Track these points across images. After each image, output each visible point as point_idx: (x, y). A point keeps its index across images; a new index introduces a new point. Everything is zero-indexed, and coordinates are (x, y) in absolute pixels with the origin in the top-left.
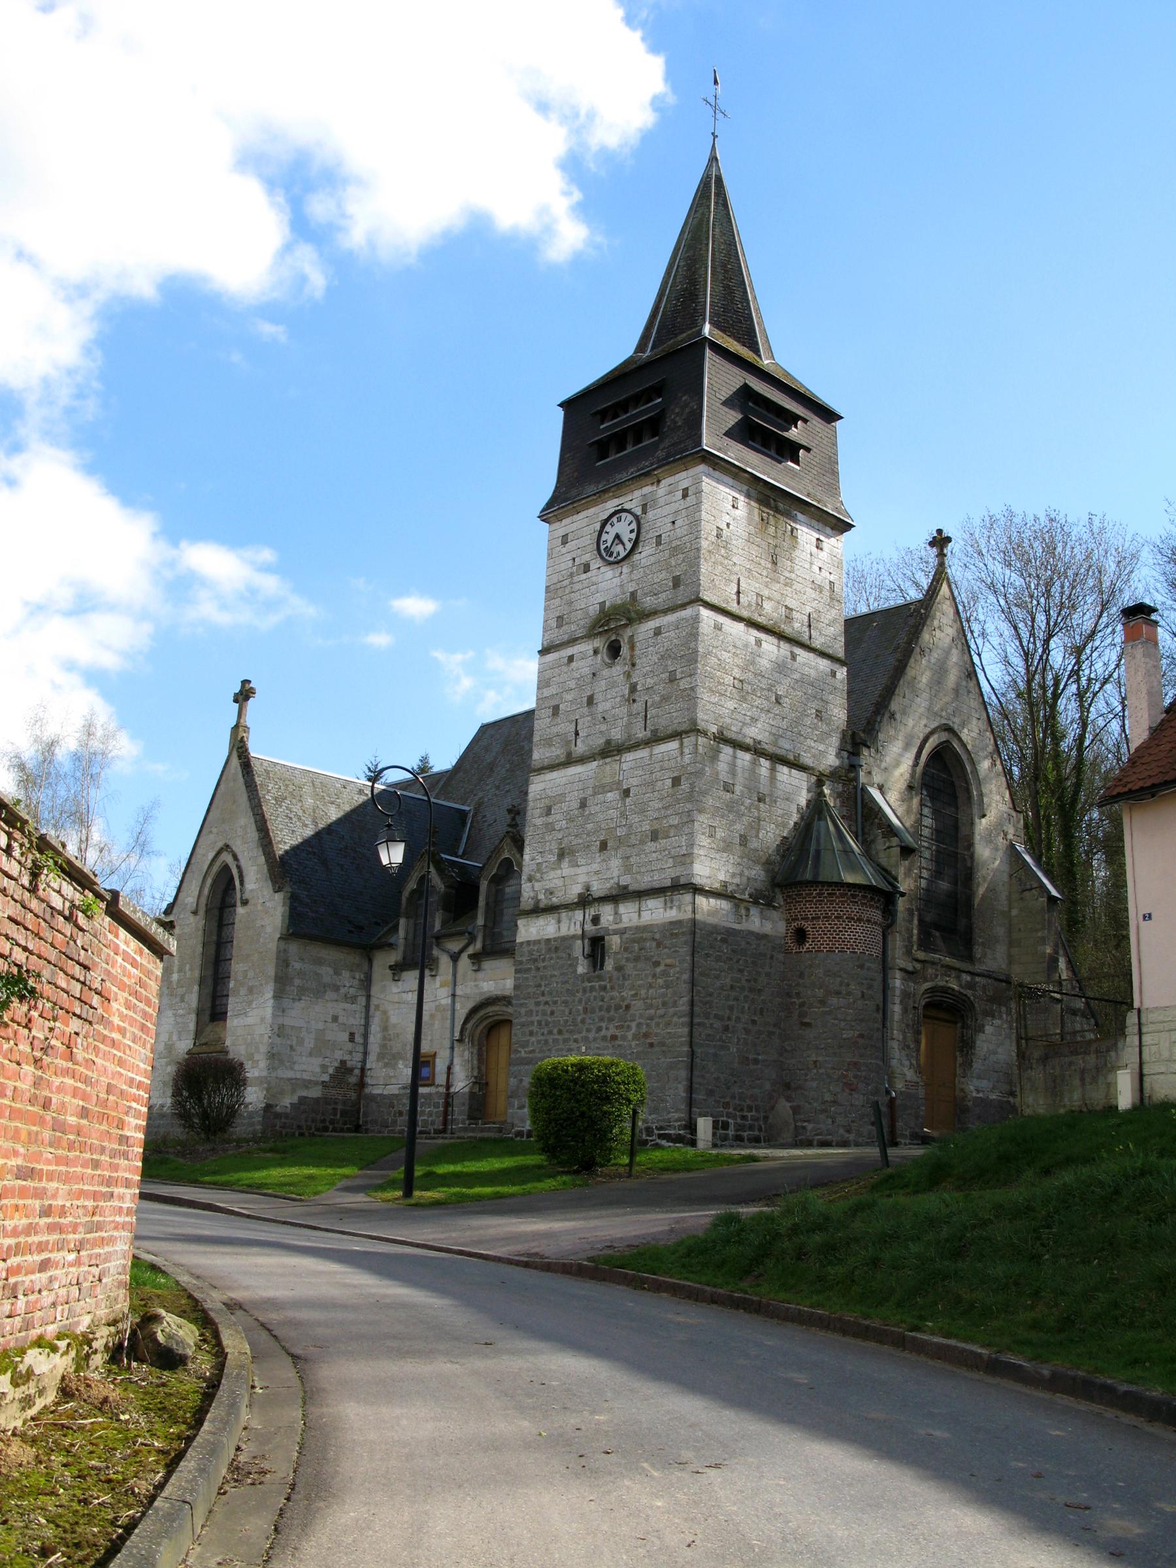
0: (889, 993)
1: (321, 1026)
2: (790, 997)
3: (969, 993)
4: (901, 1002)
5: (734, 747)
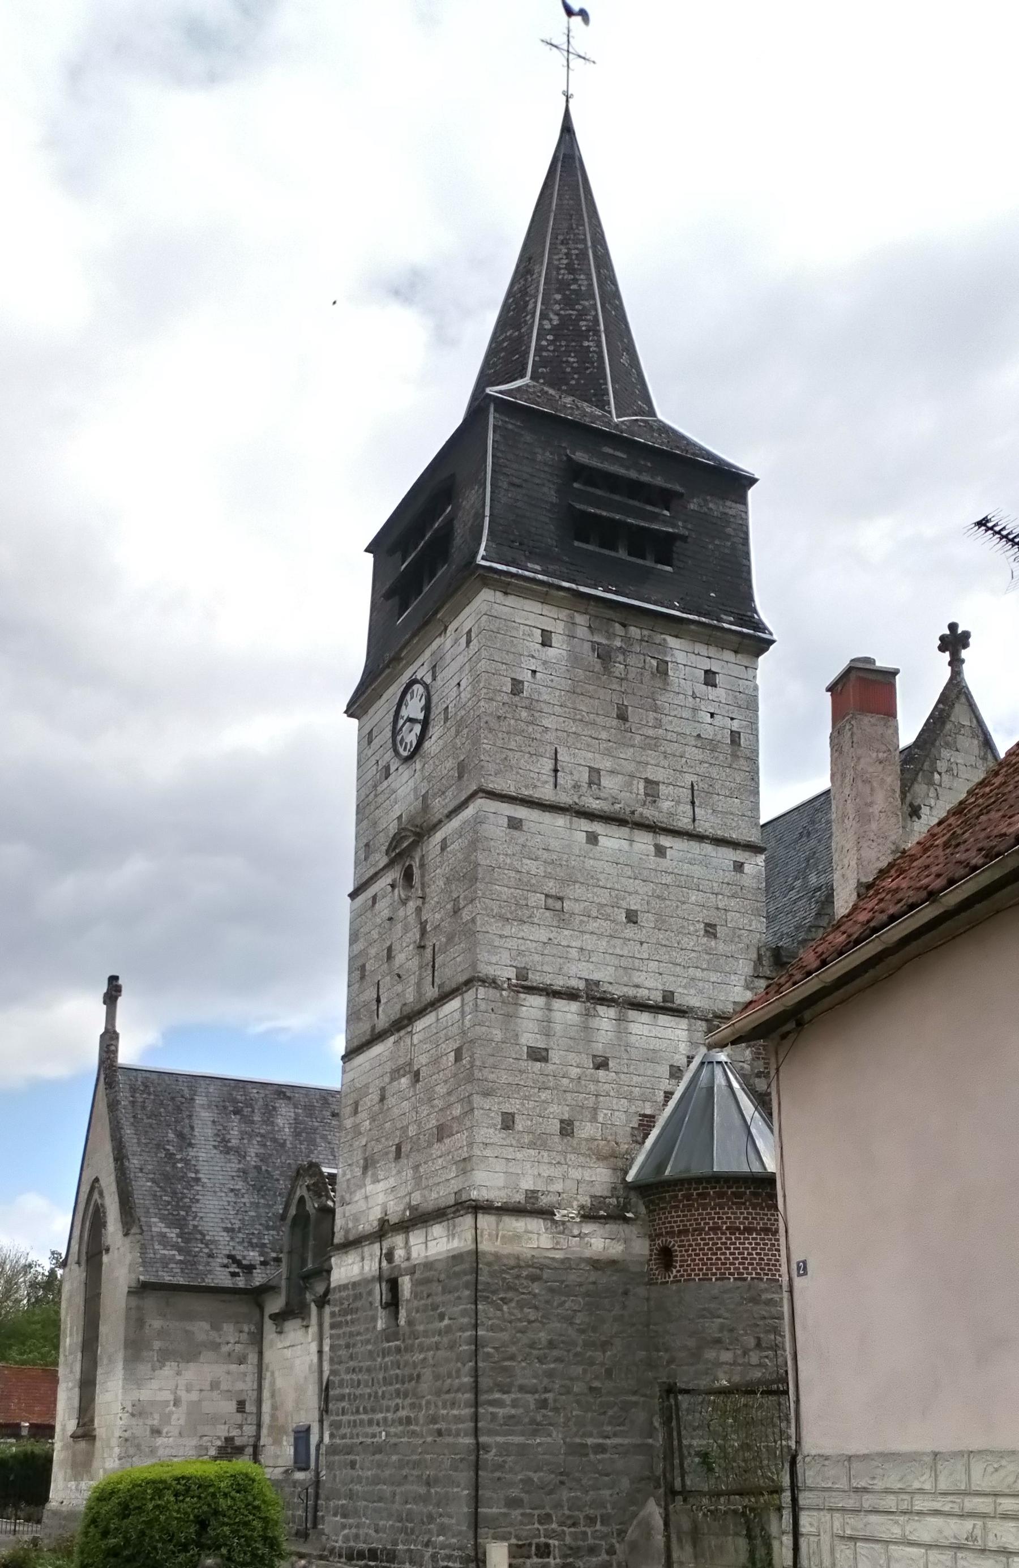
1: (194, 1396)
5: (548, 994)
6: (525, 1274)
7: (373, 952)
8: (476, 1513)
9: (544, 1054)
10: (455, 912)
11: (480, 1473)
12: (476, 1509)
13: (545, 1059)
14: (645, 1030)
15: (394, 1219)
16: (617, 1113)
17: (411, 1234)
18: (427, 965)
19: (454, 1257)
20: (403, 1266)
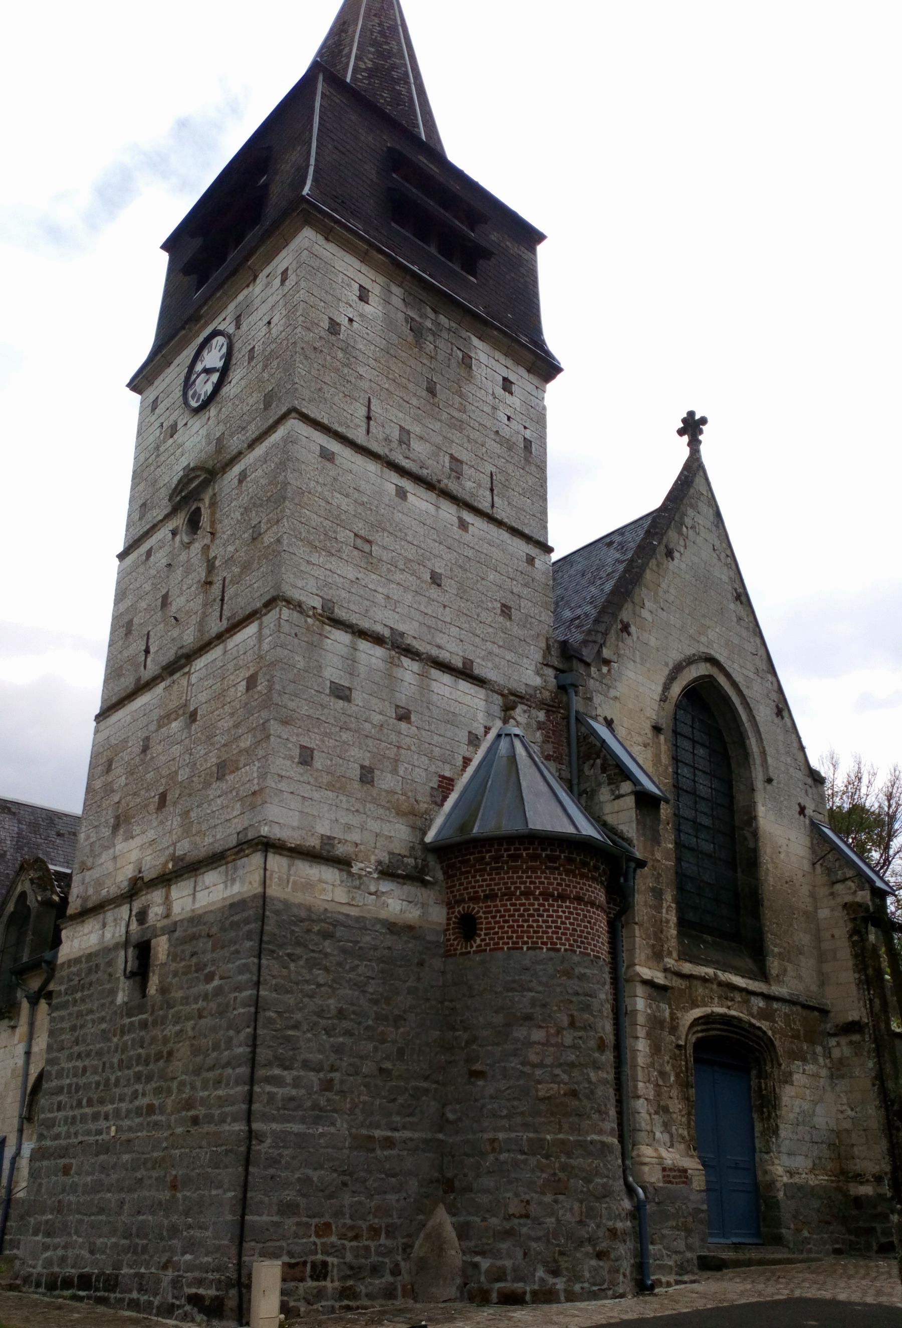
0: (627, 1022)
2: (454, 1029)
3: (764, 1025)
4: (649, 1035)
5: (353, 633)
6: (316, 928)
7: (143, 605)
8: (242, 1223)
9: (347, 693)
10: (254, 539)
11: (251, 1169)
12: (243, 1216)
13: (348, 699)
14: (446, 691)
15: (148, 875)
16: (417, 769)
17: (173, 887)
18: (215, 600)
19: (232, 905)
20: (159, 925)
